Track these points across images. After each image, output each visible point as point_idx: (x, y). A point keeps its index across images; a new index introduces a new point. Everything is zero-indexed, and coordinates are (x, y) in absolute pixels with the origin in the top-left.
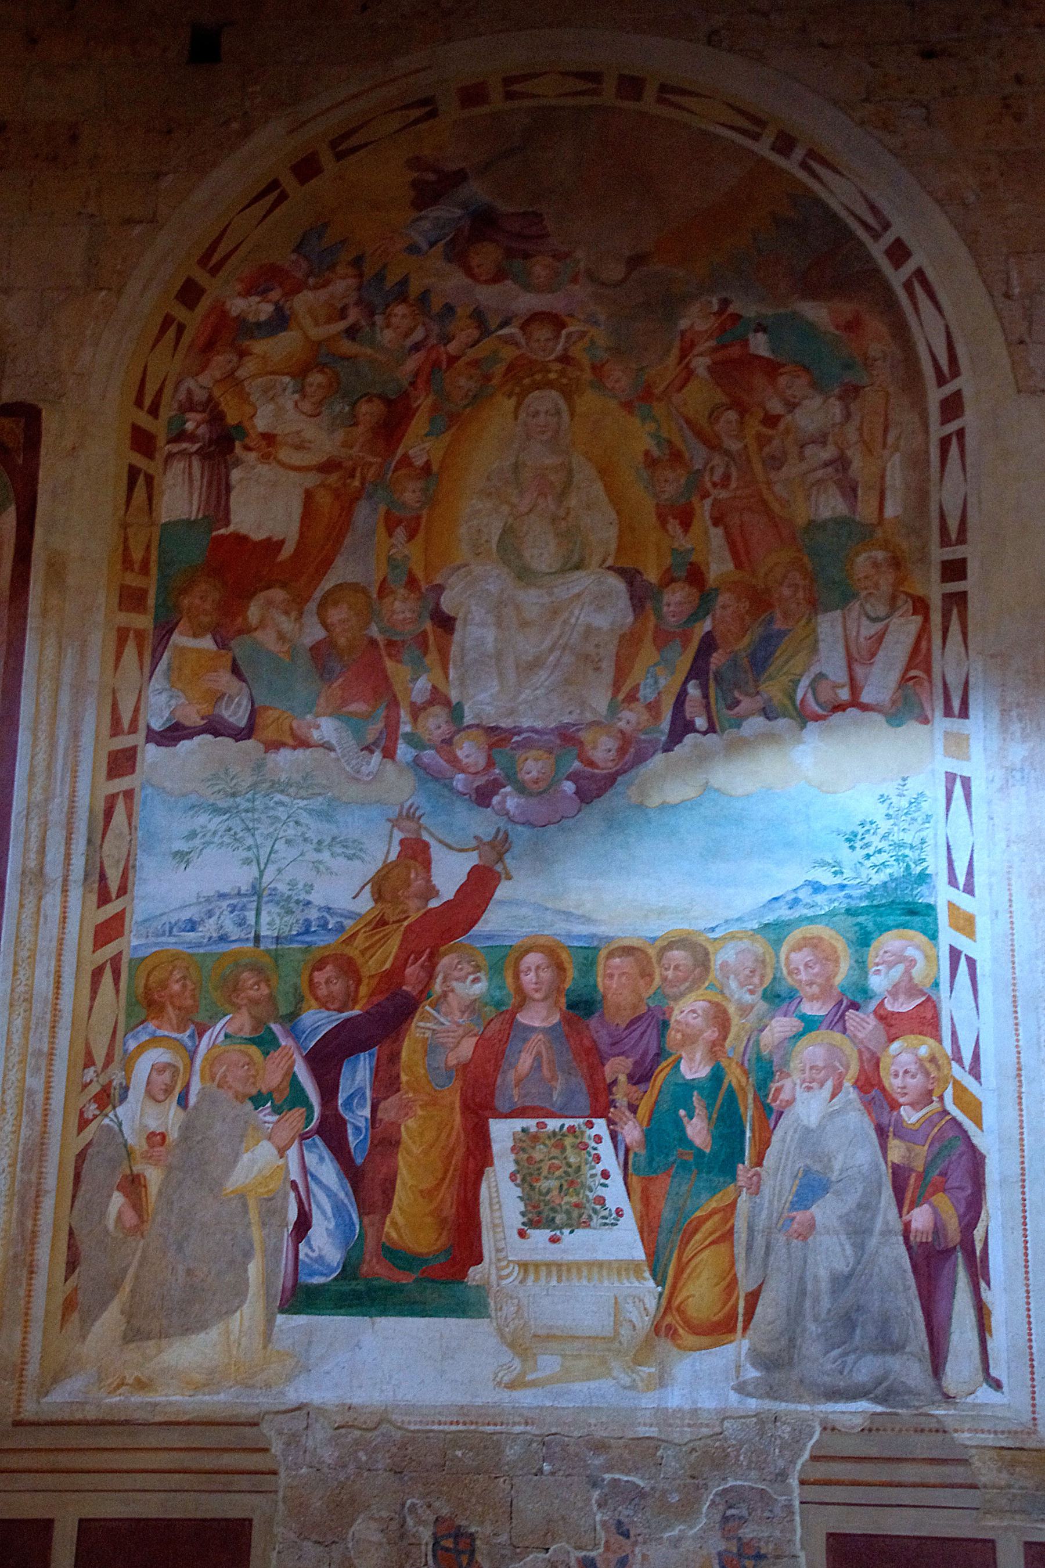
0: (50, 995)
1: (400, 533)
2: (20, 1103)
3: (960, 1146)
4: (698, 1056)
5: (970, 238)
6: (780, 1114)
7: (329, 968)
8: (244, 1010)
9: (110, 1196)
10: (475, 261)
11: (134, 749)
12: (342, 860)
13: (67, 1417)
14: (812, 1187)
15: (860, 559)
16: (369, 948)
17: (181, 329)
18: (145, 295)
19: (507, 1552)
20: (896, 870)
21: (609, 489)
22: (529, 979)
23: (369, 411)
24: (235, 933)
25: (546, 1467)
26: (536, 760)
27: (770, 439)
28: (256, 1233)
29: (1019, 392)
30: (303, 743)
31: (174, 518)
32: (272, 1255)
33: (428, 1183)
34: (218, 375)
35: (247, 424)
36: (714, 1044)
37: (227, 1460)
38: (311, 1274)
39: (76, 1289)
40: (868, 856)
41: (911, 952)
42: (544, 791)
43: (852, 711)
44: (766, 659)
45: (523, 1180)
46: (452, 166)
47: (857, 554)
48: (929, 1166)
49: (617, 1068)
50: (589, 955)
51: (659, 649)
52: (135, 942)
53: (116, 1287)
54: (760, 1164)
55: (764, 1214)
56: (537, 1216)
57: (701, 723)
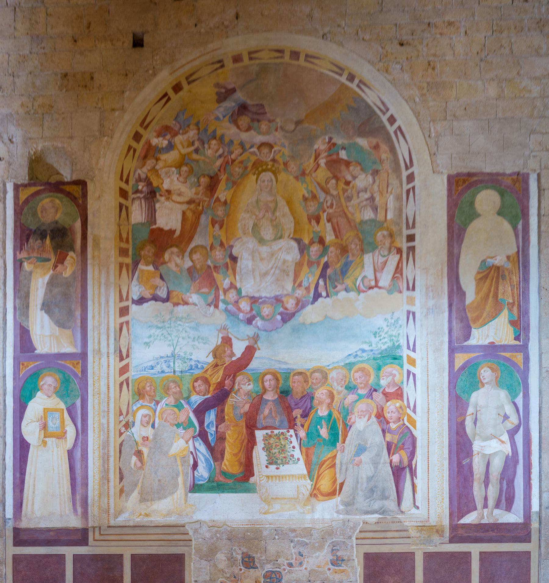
0: (106, 392)
1: (217, 226)
2: (99, 428)
3: (409, 435)
4: (324, 408)
5: (417, 115)
6: (351, 426)
7: (199, 381)
8: (172, 397)
9: (131, 457)
10: (240, 123)
11: (128, 307)
13: (124, 525)
14: (361, 449)
15: (379, 234)
16: (212, 374)
17: (135, 151)
18: (121, 138)
19: (265, 562)
20: (390, 344)
21: (291, 209)
22: (267, 384)
23: (204, 181)
24: (167, 370)
25: (277, 537)
26: (267, 308)
27: (347, 190)
28: (180, 468)
29: (434, 172)
30: (186, 303)
31: (136, 222)
32: (186, 475)
33: (236, 451)
34: (149, 168)
35: (160, 186)
36: (329, 404)
38: (199, 480)
40: (381, 340)
42: (271, 319)
43: (376, 289)
44: (346, 271)
45: (267, 450)
46: (230, 87)
47: (378, 232)
48: (398, 441)
49: (297, 413)
50: (288, 374)
51: (309, 268)
52: (133, 374)
53: (136, 485)
54: (344, 442)
55: (346, 458)
56: (271, 461)
57: (324, 294)
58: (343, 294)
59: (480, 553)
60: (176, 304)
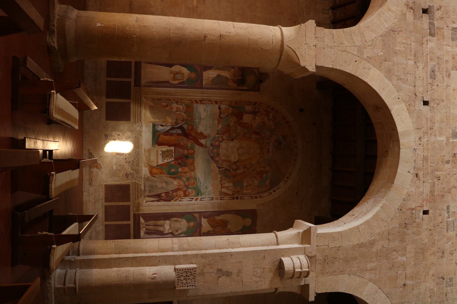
14: (167, 183)
20: (203, 192)
22: (190, 151)
30: (218, 124)
49: (180, 161)
50: (193, 158)
56: (163, 152)
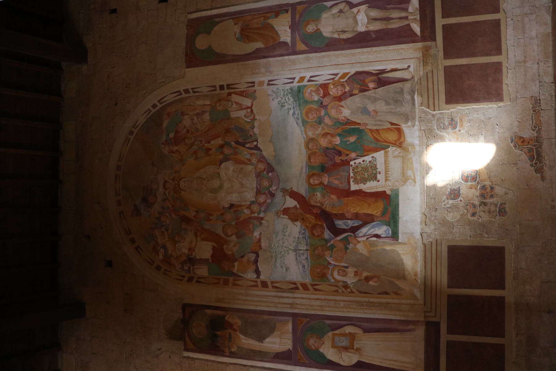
1: (211, 217)
6: (348, 119)
12: (288, 230)
14: (365, 111)
17: (166, 270)
20: (289, 96)
22: (317, 182)
24: (305, 256)
30: (260, 240)
37: (434, 252)
39: (392, 292)
41: (309, 91)
43: (253, 108)
48: (359, 84)
50: (310, 167)
52: (308, 280)
54: (359, 124)
57: (255, 143)
58: (256, 131)
59: (443, 18)
60: (260, 247)
